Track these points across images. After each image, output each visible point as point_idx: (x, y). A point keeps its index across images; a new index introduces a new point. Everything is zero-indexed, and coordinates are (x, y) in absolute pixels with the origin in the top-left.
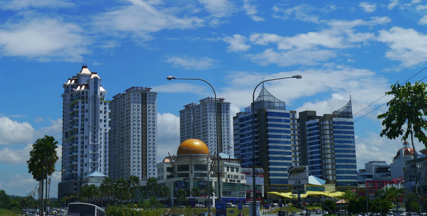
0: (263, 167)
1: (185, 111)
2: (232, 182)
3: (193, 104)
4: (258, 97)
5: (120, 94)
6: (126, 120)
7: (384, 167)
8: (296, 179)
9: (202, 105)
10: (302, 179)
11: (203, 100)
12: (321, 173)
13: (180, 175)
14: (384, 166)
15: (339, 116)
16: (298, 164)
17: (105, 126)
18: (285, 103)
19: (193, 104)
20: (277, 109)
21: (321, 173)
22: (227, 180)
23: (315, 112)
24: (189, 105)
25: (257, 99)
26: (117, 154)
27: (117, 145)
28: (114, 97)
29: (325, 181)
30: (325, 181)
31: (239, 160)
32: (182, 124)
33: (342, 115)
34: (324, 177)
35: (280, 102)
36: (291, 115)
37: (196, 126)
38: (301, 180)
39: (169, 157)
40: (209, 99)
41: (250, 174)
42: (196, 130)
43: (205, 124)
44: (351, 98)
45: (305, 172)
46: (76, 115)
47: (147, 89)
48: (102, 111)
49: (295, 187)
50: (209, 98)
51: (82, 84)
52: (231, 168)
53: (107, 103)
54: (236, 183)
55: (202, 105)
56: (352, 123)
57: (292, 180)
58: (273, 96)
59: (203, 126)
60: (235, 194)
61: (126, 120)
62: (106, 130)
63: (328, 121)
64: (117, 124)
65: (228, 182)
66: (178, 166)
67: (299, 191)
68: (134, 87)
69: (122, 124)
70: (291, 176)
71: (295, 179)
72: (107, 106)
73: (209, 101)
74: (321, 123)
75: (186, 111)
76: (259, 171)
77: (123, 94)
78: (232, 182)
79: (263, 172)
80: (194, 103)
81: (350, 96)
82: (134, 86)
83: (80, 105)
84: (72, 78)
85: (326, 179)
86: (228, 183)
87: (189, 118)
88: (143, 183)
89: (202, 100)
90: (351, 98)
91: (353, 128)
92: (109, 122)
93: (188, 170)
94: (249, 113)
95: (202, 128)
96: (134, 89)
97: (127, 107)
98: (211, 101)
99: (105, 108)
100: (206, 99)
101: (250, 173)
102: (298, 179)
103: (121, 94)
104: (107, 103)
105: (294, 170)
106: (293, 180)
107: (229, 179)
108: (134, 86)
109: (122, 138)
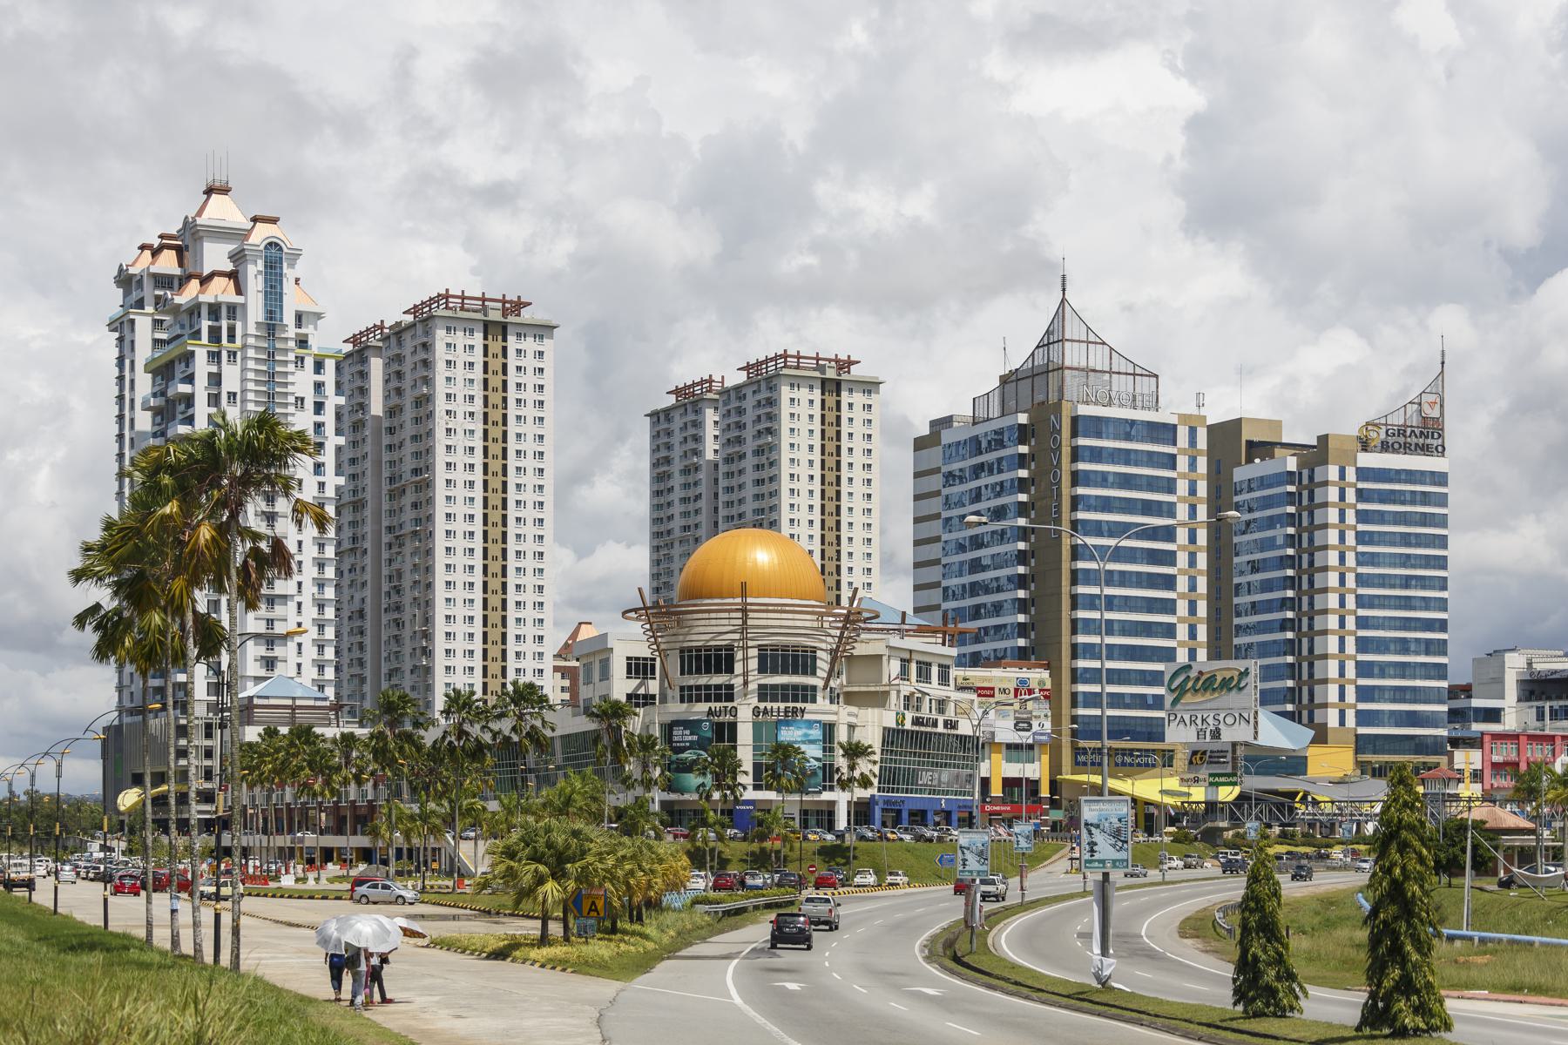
0: (1047, 667)
1: (749, 391)
2: (923, 729)
3: (710, 381)
4: (1038, 347)
5: (382, 327)
6: (409, 448)
7: (1554, 676)
8: (1203, 720)
9: (755, 387)
10: (1230, 720)
11: (759, 363)
12: (1292, 695)
13: (689, 695)
14: (1556, 672)
15: (1385, 447)
16: (1202, 655)
17: (318, 468)
18: (1156, 376)
19: (710, 381)
20: (1121, 405)
21: (1292, 695)
22: (901, 719)
23: (1276, 425)
24: (694, 384)
25: (1033, 354)
26: (368, 601)
27: (368, 560)
28: (354, 340)
29: (1311, 733)
30: (1311, 733)
31: (944, 633)
32: (658, 471)
33: (1402, 439)
34: (1305, 713)
35: (1138, 371)
36: (1183, 434)
37: (723, 483)
38: (1222, 726)
39: (640, 609)
40: (785, 362)
41: (993, 696)
42: (722, 498)
43: (765, 474)
44: (1443, 363)
45: (1245, 691)
46: (180, 417)
47: (508, 305)
48: (302, 399)
49: (1194, 753)
50: (785, 356)
51: (206, 272)
52: (940, 666)
53: (330, 365)
54: (940, 734)
55: (755, 387)
56: (1440, 478)
57: (1182, 725)
58: (1104, 343)
59: (759, 482)
60: (935, 783)
61: (409, 448)
62: (322, 485)
63: (1337, 468)
64: (368, 464)
65: (908, 726)
66: (761, 648)
67: (1211, 775)
68: (447, 296)
69: (392, 463)
70: (1179, 707)
71: (1199, 721)
72: (329, 376)
73: (785, 371)
74: (1305, 473)
75: (754, 392)
76: (1034, 685)
77: (398, 324)
78: (923, 729)
79: (1048, 686)
80: (717, 378)
81: (1440, 353)
82: (447, 290)
83: (202, 367)
84: (156, 242)
85: (1311, 723)
86: (908, 731)
87: (691, 445)
88: (566, 724)
89: (753, 361)
90: (1443, 363)
91: (1442, 500)
92: (339, 449)
93: (730, 670)
94: (988, 419)
95: (750, 491)
96: (447, 303)
97: (414, 386)
98: (797, 368)
99: (319, 386)
100: (776, 358)
101: (993, 689)
102: (1210, 720)
103: (387, 324)
104: (330, 365)
105: (1198, 679)
106: (1188, 722)
107: (909, 716)
108: (447, 290)
109: (390, 529)
